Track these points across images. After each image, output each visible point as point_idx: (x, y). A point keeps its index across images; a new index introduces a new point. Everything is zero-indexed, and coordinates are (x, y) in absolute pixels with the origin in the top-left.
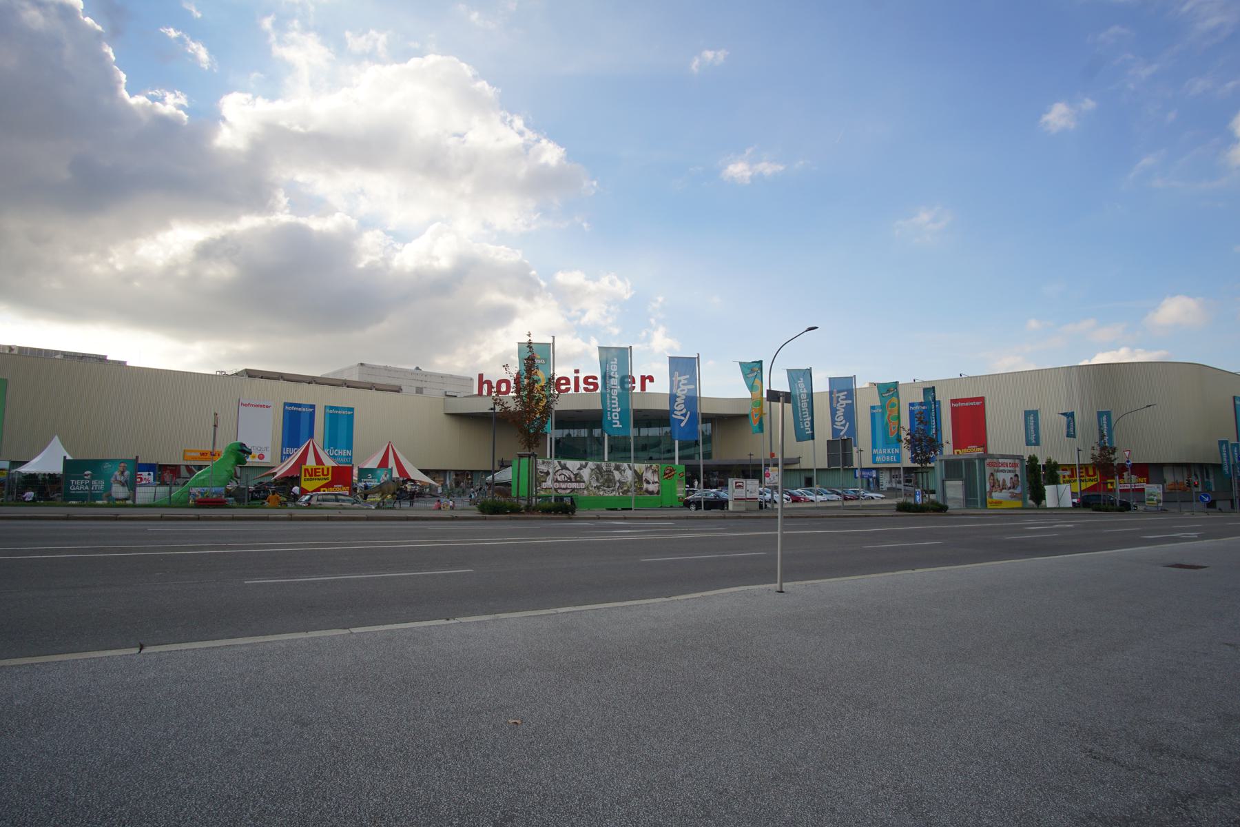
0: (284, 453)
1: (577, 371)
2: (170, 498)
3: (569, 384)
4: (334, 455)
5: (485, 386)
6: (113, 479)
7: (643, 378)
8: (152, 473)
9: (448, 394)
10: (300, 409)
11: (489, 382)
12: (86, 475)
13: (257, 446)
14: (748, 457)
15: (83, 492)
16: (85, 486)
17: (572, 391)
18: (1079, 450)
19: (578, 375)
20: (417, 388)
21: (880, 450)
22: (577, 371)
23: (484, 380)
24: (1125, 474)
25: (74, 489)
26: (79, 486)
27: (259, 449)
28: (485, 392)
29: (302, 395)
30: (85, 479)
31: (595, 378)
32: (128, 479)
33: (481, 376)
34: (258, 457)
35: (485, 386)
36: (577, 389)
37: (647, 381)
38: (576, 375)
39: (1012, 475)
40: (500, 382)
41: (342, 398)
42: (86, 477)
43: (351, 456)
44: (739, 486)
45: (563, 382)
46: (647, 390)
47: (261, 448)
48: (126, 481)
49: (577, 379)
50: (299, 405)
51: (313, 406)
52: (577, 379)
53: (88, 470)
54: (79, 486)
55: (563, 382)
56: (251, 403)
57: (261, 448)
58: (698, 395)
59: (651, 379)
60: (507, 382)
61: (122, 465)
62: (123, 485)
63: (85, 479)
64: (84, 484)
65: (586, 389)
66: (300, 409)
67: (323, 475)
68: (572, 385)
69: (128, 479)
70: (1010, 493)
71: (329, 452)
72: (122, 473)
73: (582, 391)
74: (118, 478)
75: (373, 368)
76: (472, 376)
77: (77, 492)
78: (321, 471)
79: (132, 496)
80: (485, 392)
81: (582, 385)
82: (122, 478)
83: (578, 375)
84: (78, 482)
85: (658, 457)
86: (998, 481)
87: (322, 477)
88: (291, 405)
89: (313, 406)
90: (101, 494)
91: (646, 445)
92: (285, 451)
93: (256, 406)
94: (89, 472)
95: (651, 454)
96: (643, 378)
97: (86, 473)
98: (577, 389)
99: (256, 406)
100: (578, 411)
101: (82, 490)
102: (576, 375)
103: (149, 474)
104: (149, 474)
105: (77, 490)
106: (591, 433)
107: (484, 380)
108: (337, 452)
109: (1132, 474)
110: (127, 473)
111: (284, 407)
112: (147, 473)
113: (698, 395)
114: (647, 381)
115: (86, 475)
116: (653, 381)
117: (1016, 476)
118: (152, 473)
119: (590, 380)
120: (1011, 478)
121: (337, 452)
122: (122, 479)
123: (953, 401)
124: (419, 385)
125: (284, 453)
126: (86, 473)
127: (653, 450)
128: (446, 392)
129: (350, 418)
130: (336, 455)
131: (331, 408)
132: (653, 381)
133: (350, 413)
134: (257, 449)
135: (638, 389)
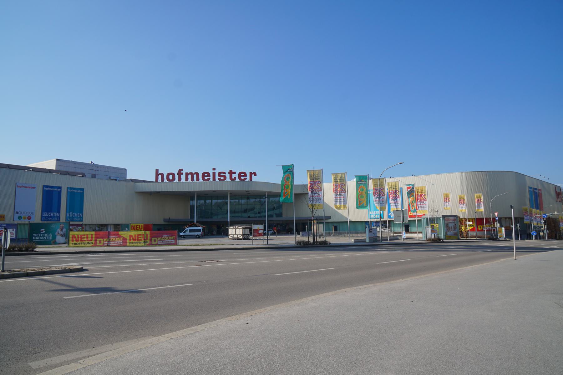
0: (43, 216)
1: (214, 169)
2: (309, 238)
3: (210, 176)
4: (49, 216)
5: (160, 177)
6: (56, 233)
7: (251, 174)
8: (15, 229)
9: (111, 178)
10: (52, 189)
11: (162, 175)
12: (41, 231)
13: (27, 212)
14: (318, 216)
15: (40, 240)
16: (41, 237)
17: (211, 180)
18: (475, 213)
19: (215, 171)
20: (92, 174)
21: (373, 212)
22: (214, 169)
23: (159, 173)
24: (496, 223)
25: (35, 239)
26: (38, 237)
27: (28, 213)
28: (160, 180)
29: (54, 181)
30: (41, 233)
31: (225, 173)
32: (65, 233)
33: (157, 171)
34: (28, 218)
35: (160, 177)
36: (214, 179)
37: (253, 175)
38: (213, 171)
39: (454, 224)
40: (168, 175)
41: (76, 182)
42: (41, 232)
43: (82, 217)
44: (371, 231)
45: (206, 175)
46: (253, 180)
47: (30, 213)
48: (64, 234)
49: (214, 174)
50: (52, 187)
51: (60, 188)
52: (214, 174)
53: (43, 228)
54: (38, 237)
55: (206, 175)
56: (23, 186)
57: (30, 213)
58: (368, 189)
59: (255, 174)
60: (173, 175)
61: (62, 225)
62: (62, 236)
63: (41, 233)
64: (40, 236)
65: (219, 179)
66: (52, 189)
67: (140, 229)
68: (211, 177)
69: (65, 233)
70: (453, 232)
71: (69, 215)
72: (62, 230)
73: (217, 180)
74: (60, 232)
75: (65, 162)
76: (126, 168)
77: (42, 240)
78: (139, 227)
79: (67, 241)
80: (160, 180)
81: (217, 177)
82: (62, 232)
83: (215, 171)
84: (37, 235)
85: (253, 216)
86: (449, 227)
87: (139, 230)
88: (47, 187)
89: (60, 188)
90: (50, 241)
91: (246, 209)
92: (44, 215)
93: (27, 187)
94: (126, 228)
95: (249, 215)
96: (251, 174)
97: (41, 230)
98: (214, 179)
99: (27, 187)
100: (214, 191)
101: (39, 239)
102: (213, 171)
103: (13, 230)
104: (13, 230)
105: (37, 239)
106: (205, 202)
107: (159, 173)
108: (50, 214)
109: (498, 223)
110: (64, 230)
111: (43, 188)
112: (12, 229)
113: (368, 189)
114: (253, 175)
115: (41, 231)
116: (256, 176)
117: (455, 225)
118: (15, 229)
119: (222, 174)
120: (454, 226)
121: (74, 215)
122: (62, 233)
123: (44, 186)
124: (94, 172)
125: (43, 216)
126: (41, 230)
127: (250, 212)
128: (110, 177)
129: (82, 195)
130: (74, 216)
131: (71, 188)
132: (256, 176)
133: (81, 191)
134: (27, 213)
135: (248, 179)
